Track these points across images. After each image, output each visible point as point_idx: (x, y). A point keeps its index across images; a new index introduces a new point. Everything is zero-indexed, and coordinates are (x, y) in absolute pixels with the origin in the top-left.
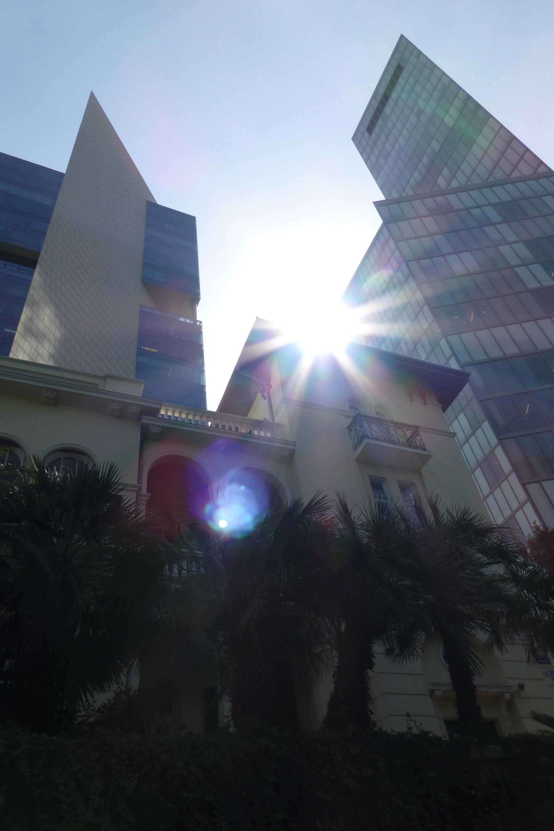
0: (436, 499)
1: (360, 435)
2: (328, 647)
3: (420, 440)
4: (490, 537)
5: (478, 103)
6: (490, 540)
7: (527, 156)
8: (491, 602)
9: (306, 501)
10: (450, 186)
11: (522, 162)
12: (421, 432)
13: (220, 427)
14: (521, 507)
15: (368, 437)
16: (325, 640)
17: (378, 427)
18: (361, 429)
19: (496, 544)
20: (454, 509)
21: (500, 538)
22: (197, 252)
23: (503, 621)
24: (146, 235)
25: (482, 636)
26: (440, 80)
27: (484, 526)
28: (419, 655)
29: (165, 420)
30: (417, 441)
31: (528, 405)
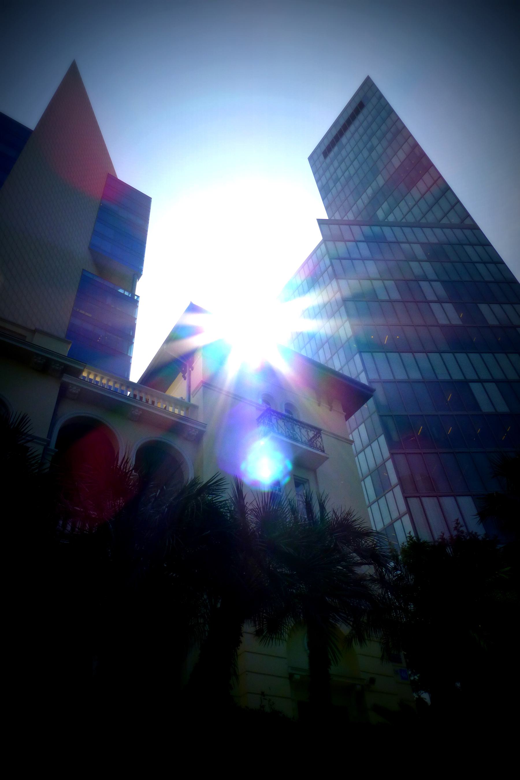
2: (201, 621)
3: (320, 442)
4: (367, 540)
6: (366, 542)
12: (323, 435)
13: (138, 398)
14: (400, 518)
19: (370, 547)
21: (375, 542)
22: (147, 231)
24: (101, 205)
25: (345, 629)
27: (363, 529)
28: (285, 640)
30: (317, 442)
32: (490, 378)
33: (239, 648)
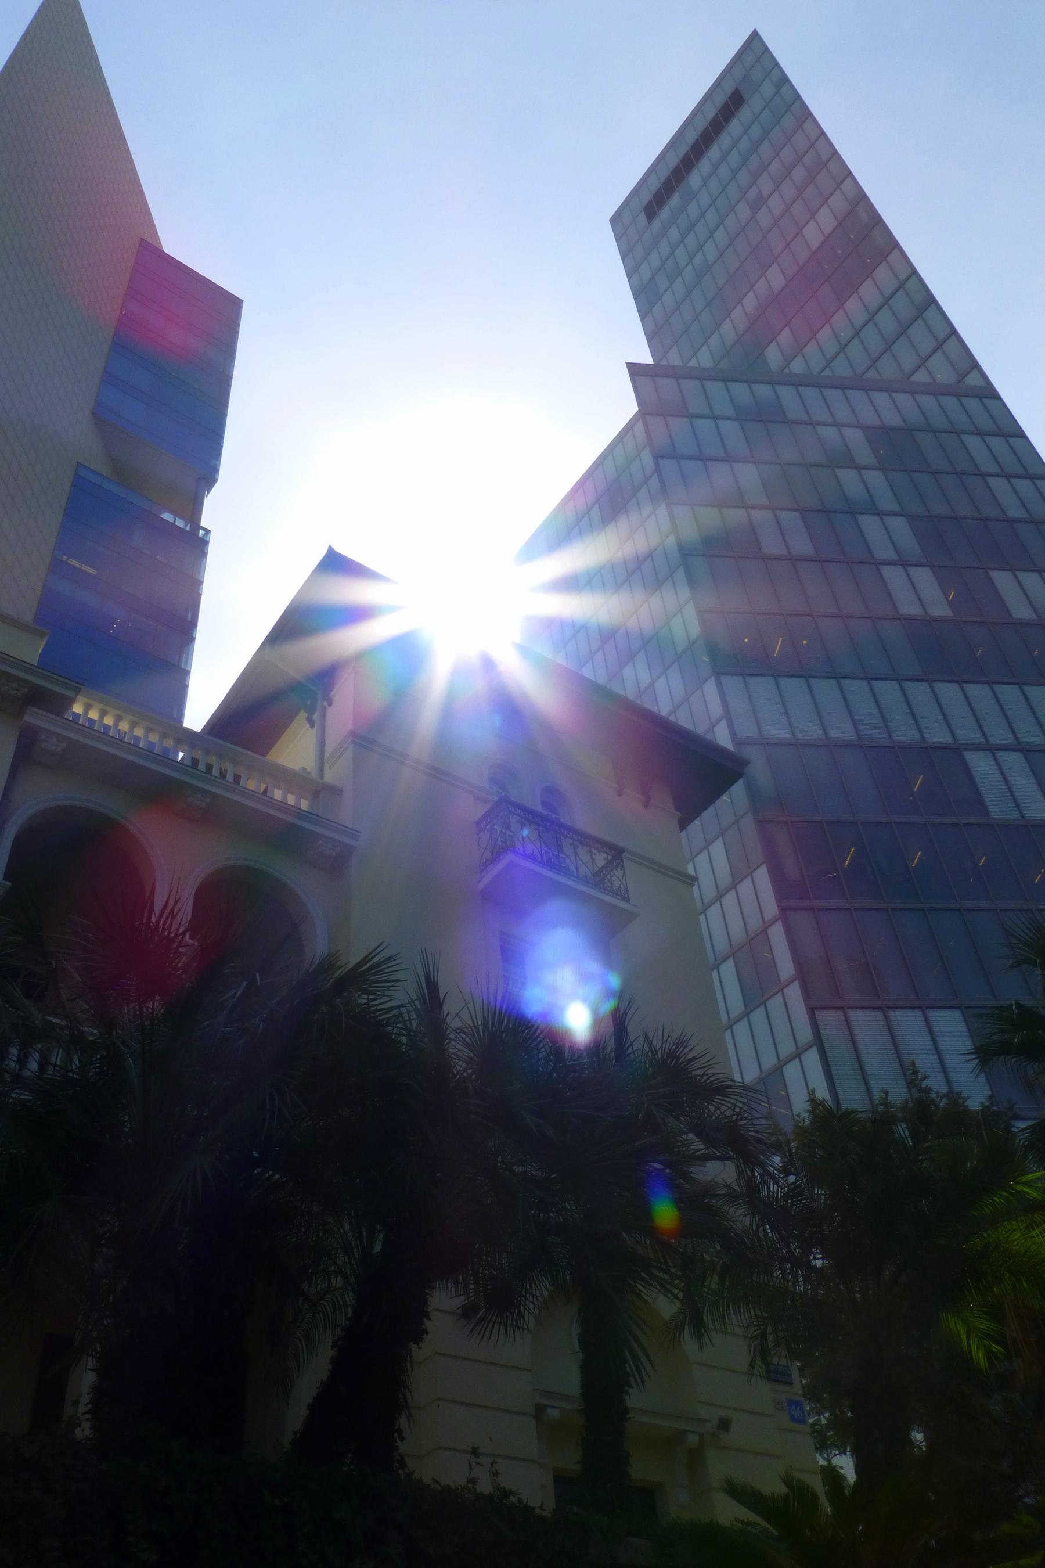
0: (628, 1005)
1: (499, 842)
4: (720, 1103)
5: (878, 214)
6: (717, 1108)
7: (951, 345)
8: (694, 1239)
9: (353, 958)
10: (789, 368)
11: (939, 355)
13: (202, 767)
14: (798, 1055)
15: (516, 852)
16: (336, 1267)
17: (539, 833)
18: (503, 830)
19: (726, 1120)
20: (660, 1033)
21: (737, 1110)
22: (231, 378)
23: (713, 1282)
24: (124, 312)
26: (812, 145)
27: (712, 1079)
28: (529, 1330)
29: (81, 728)
31: (853, 850)
33: (420, 1346)
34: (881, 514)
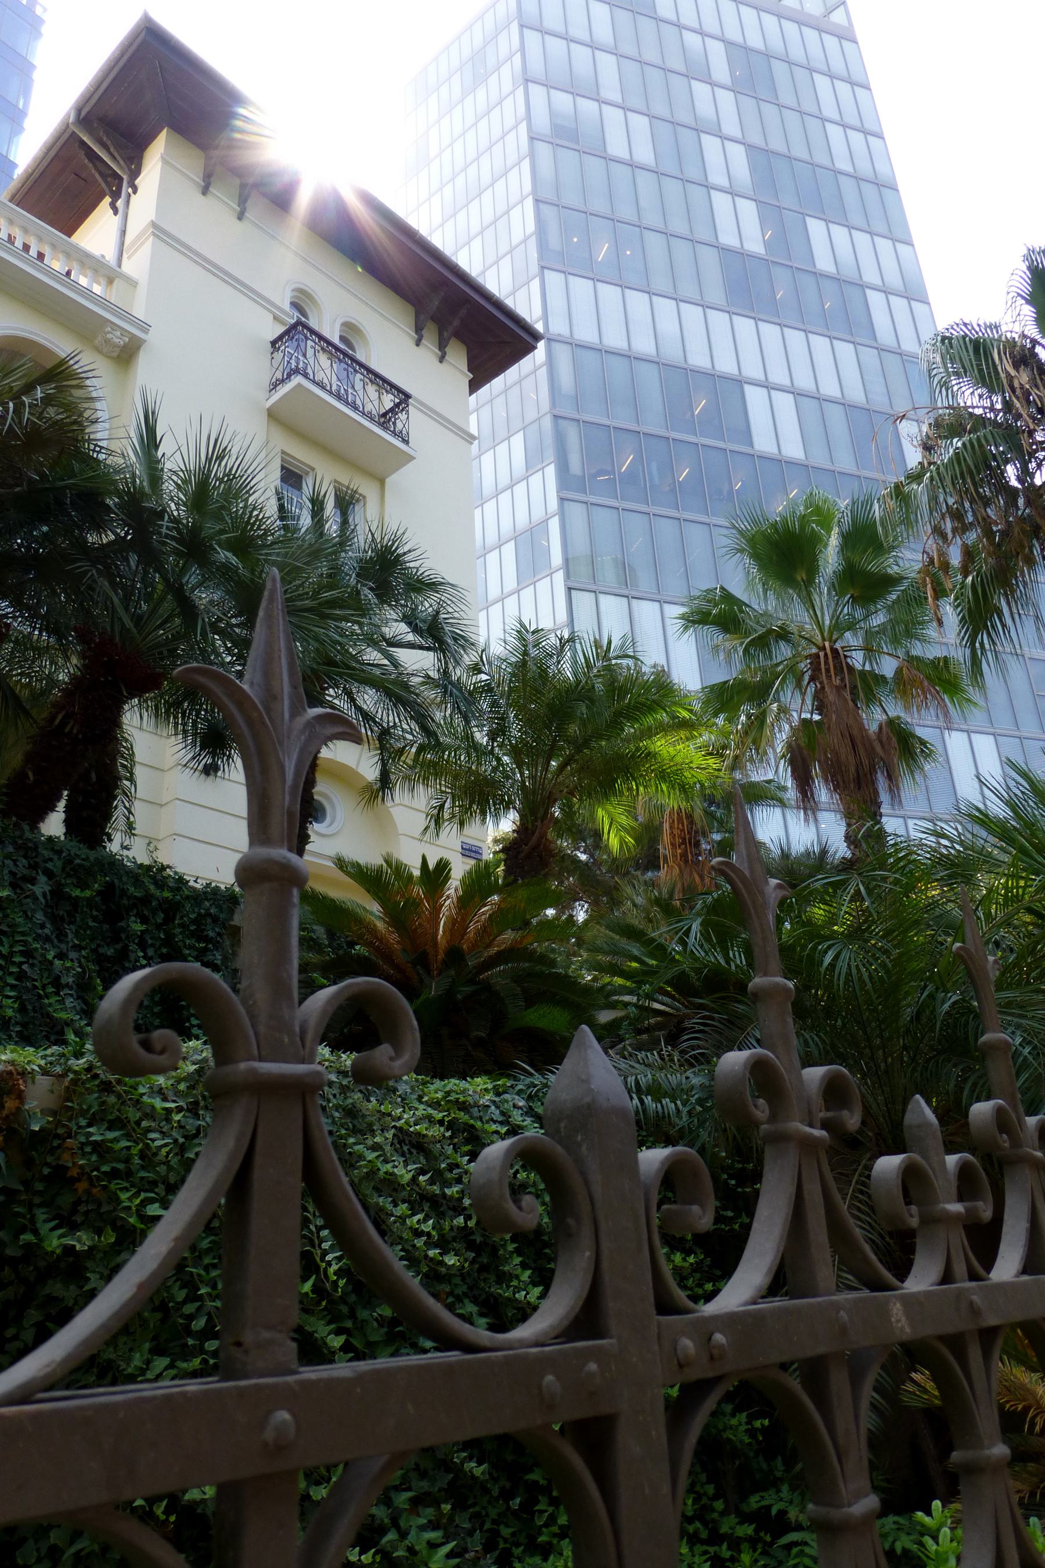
15: (306, 376)
32: (697, 26)
34: (723, 138)
